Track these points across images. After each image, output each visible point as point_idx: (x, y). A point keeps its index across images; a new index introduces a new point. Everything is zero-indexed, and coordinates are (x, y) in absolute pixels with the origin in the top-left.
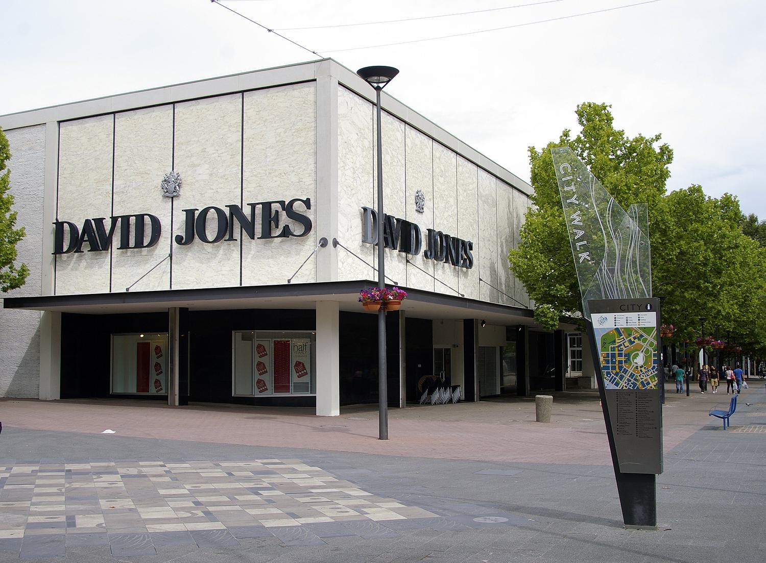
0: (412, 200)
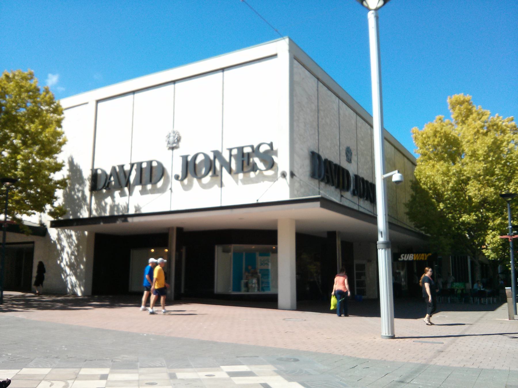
0: (344, 153)
